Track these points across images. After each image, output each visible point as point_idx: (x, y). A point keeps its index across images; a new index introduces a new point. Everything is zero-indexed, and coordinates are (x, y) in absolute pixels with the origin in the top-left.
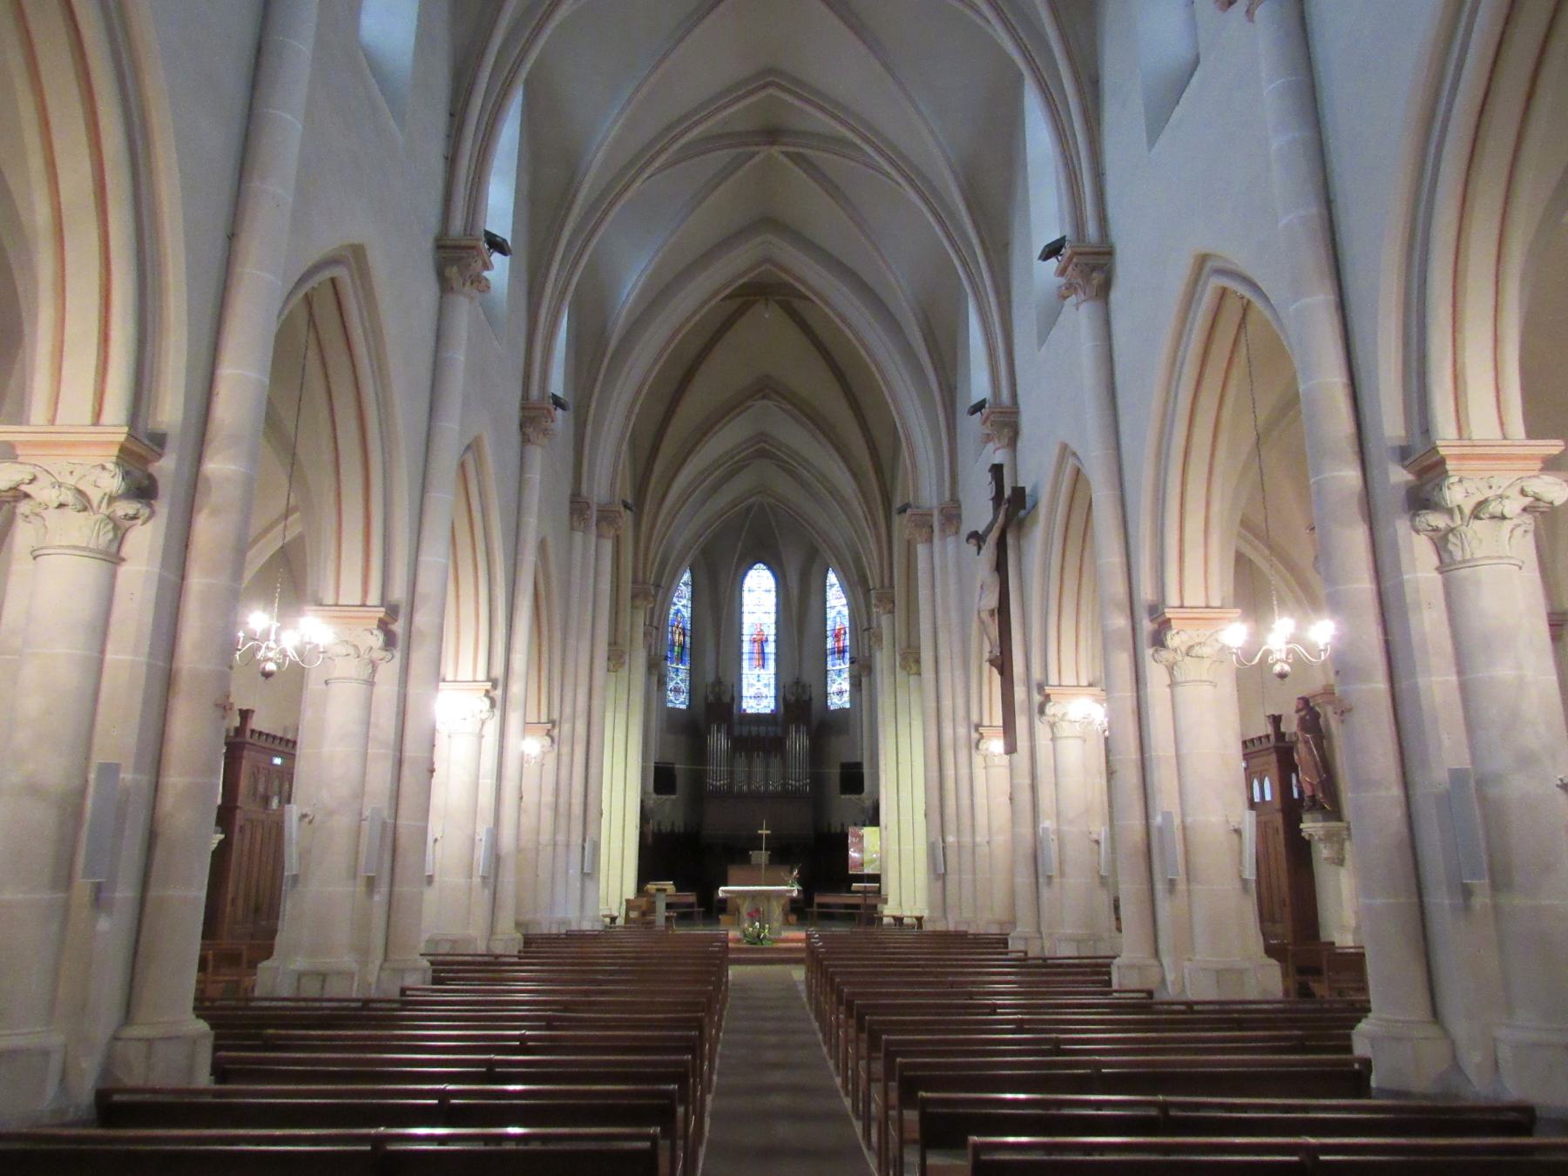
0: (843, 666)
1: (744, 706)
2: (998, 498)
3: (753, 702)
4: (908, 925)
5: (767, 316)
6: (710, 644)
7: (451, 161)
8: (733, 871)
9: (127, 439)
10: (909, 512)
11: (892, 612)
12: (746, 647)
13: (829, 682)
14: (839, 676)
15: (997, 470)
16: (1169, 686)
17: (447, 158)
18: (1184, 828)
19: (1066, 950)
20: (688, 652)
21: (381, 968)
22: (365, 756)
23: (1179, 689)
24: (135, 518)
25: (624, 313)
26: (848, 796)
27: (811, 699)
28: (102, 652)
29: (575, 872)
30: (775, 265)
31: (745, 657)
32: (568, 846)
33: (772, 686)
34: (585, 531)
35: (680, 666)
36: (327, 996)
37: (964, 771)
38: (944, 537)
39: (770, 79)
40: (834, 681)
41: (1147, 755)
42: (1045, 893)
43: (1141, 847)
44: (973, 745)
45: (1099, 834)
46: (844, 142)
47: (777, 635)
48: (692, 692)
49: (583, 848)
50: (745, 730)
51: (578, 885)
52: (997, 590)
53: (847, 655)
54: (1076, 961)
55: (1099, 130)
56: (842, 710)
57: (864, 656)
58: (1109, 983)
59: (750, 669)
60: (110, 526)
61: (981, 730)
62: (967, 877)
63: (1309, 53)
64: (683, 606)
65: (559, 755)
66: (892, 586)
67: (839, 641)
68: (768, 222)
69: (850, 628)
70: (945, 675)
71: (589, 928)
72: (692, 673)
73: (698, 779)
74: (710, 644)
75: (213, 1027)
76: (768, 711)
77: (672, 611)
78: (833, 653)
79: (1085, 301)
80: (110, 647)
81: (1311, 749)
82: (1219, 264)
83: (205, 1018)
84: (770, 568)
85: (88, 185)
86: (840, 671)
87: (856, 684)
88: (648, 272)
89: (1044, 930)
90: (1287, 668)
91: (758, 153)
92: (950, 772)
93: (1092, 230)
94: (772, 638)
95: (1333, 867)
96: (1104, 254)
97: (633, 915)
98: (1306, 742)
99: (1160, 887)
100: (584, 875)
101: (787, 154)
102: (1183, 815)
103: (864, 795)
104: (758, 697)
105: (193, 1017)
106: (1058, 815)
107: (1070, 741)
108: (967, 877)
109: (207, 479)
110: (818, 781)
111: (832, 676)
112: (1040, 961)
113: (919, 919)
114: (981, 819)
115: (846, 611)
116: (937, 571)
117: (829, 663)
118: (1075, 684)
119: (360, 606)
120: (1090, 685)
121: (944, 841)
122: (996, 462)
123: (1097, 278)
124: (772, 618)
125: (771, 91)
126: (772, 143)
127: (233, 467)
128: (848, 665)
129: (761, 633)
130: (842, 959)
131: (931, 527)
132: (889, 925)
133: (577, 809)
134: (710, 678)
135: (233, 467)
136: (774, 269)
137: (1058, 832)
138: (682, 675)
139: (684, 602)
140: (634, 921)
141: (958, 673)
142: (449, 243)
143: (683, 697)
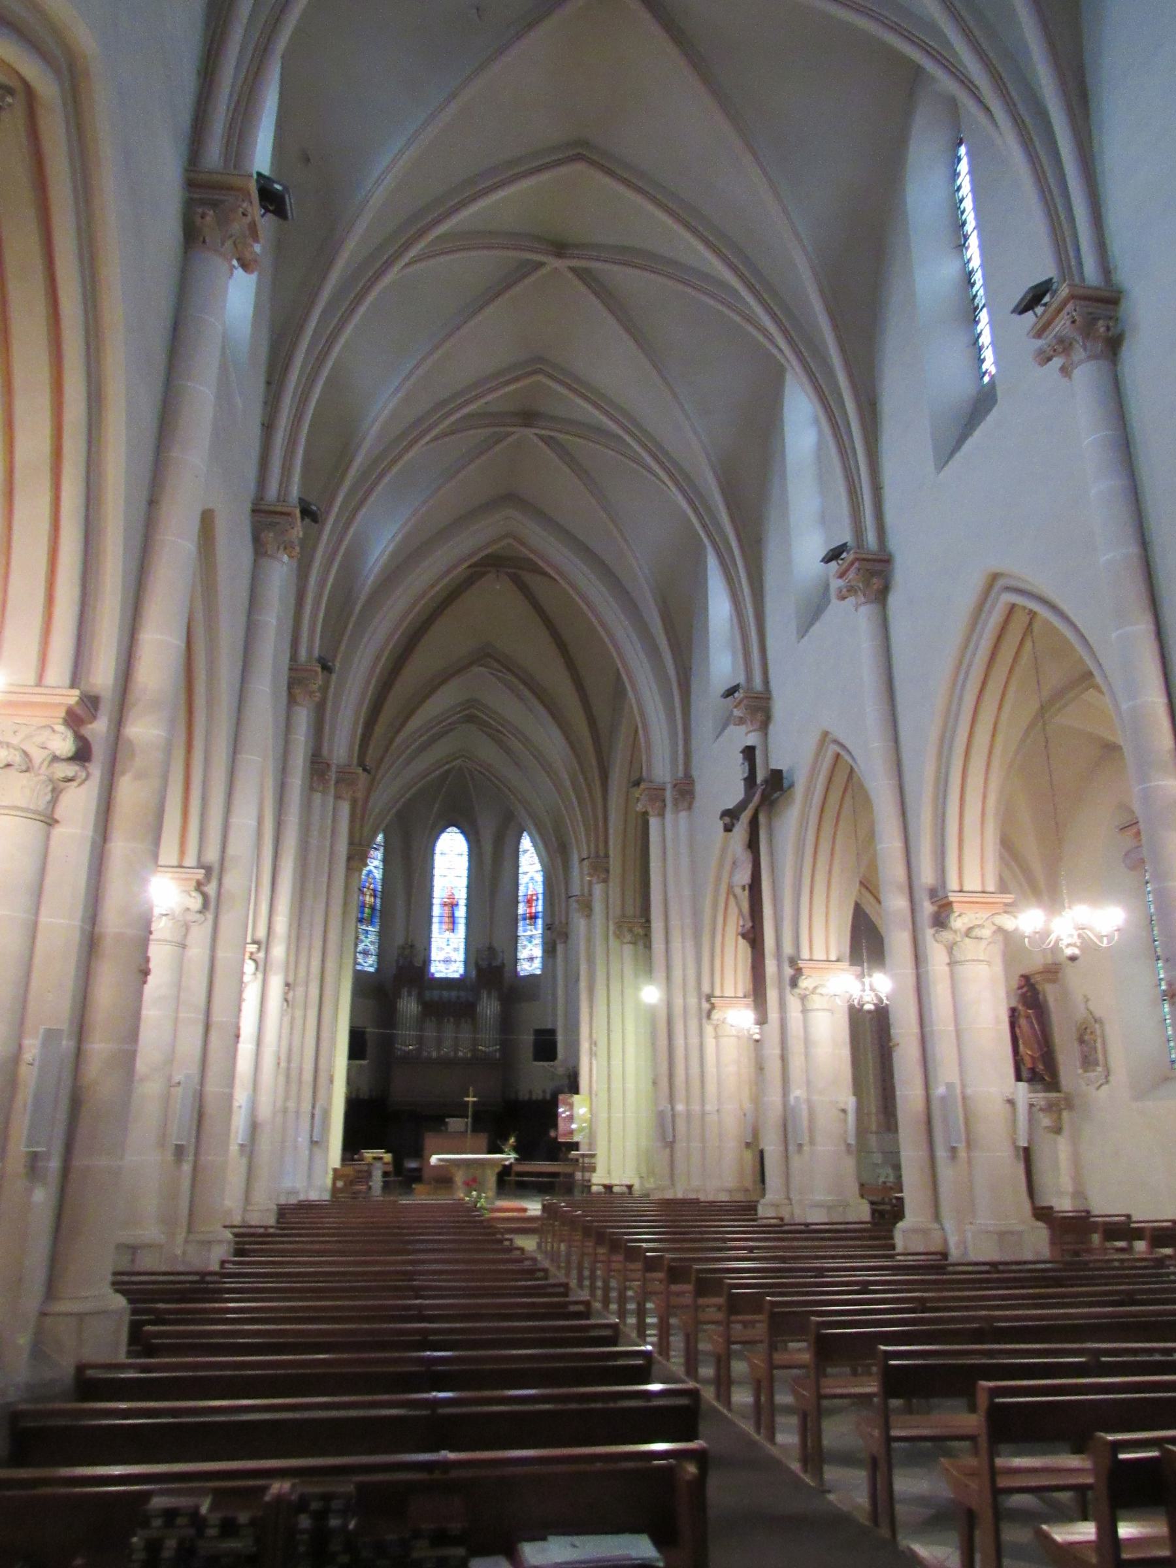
0: (534, 932)
1: (433, 969)
2: (750, 781)
3: (442, 967)
4: (617, 1193)
5: (498, 587)
6: (400, 902)
7: (268, 428)
8: (430, 1140)
9: (77, 703)
10: (642, 786)
11: (605, 881)
12: (437, 910)
13: (519, 948)
14: (530, 942)
15: (749, 753)
16: (949, 964)
17: (263, 425)
18: (964, 1098)
19: (816, 1217)
20: (378, 914)
21: (186, 1242)
22: (176, 1020)
23: (959, 969)
24: (71, 780)
25: (372, 578)
26: (541, 1063)
27: (503, 965)
28: (37, 913)
29: (303, 1140)
30: (515, 538)
31: (435, 920)
32: (297, 1112)
33: (462, 951)
34: (324, 793)
35: (370, 928)
36: (137, 1268)
37: (694, 1040)
38: (677, 810)
39: (539, 366)
40: (524, 947)
41: (927, 1029)
42: (796, 1161)
43: (923, 1118)
44: (704, 1014)
45: (846, 1103)
46: (600, 431)
47: (468, 899)
48: (380, 956)
49: (313, 1116)
50: (435, 995)
51: (307, 1152)
52: (750, 866)
53: (540, 922)
54: (827, 1227)
55: (877, 448)
56: (533, 976)
57: (561, 923)
58: (893, 1247)
59: (440, 933)
60: (50, 788)
61: (713, 1000)
62: (696, 1144)
63: (1123, 412)
64: (375, 867)
65: (293, 1019)
66: (607, 856)
67: (530, 907)
68: (511, 498)
69: (544, 894)
70: (676, 944)
71: (316, 1199)
72: (382, 935)
73: (387, 1043)
74: (400, 902)
75: (130, 1301)
76: (457, 975)
77: (364, 872)
78: (525, 919)
79: (864, 603)
80: (44, 911)
81: (1032, 1023)
82: (1013, 583)
83: (123, 1293)
84: (463, 832)
85: (46, 447)
86: (531, 937)
87: (550, 950)
88: (397, 539)
89: (795, 1196)
90: (1076, 951)
91: (513, 433)
92: (679, 1042)
93: (871, 538)
94: (462, 902)
95: (1052, 1136)
96: (880, 561)
97: (340, 1184)
98: (1028, 1017)
99: (941, 1153)
100: (314, 1143)
101: (541, 438)
102: (963, 1086)
103: (556, 1063)
104: (447, 961)
105: (111, 1291)
106: (808, 1083)
107: (819, 1014)
108: (696, 1144)
109: (130, 741)
110: (507, 1047)
111: (522, 942)
112: (803, 1227)
113: (630, 1187)
114: (711, 1088)
115: (539, 878)
116: (669, 844)
117: (520, 929)
118: (825, 958)
119: (177, 867)
120: (838, 960)
121: (673, 1109)
122: (749, 744)
123: (876, 582)
124: (464, 882)
125: (541, 378)
126: (527, 425)
127: (155, 732)
128: (540, 931)
129: (452, 896)
130: (688, 1221)
131: (664, 801)
132: (599, 1193)
133: (308, 1076)
134: (399, 940)
135: (155, 732)
136: (515, 544)
137: (808, 1101)
138: (372, 937)
139: (376, 863)
140: (341, 1190)
141: (690, 944)
142: (263, 507)
143: (372, 960)
